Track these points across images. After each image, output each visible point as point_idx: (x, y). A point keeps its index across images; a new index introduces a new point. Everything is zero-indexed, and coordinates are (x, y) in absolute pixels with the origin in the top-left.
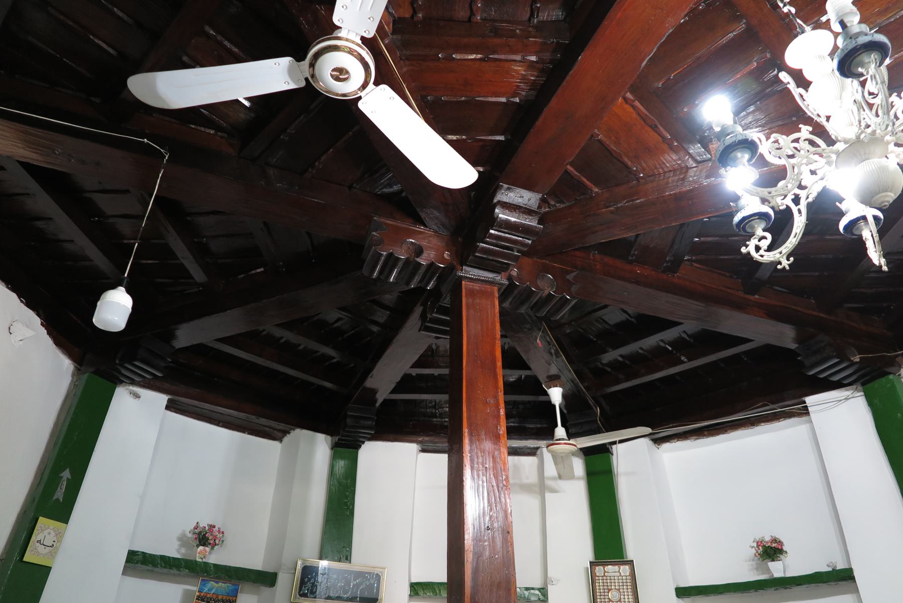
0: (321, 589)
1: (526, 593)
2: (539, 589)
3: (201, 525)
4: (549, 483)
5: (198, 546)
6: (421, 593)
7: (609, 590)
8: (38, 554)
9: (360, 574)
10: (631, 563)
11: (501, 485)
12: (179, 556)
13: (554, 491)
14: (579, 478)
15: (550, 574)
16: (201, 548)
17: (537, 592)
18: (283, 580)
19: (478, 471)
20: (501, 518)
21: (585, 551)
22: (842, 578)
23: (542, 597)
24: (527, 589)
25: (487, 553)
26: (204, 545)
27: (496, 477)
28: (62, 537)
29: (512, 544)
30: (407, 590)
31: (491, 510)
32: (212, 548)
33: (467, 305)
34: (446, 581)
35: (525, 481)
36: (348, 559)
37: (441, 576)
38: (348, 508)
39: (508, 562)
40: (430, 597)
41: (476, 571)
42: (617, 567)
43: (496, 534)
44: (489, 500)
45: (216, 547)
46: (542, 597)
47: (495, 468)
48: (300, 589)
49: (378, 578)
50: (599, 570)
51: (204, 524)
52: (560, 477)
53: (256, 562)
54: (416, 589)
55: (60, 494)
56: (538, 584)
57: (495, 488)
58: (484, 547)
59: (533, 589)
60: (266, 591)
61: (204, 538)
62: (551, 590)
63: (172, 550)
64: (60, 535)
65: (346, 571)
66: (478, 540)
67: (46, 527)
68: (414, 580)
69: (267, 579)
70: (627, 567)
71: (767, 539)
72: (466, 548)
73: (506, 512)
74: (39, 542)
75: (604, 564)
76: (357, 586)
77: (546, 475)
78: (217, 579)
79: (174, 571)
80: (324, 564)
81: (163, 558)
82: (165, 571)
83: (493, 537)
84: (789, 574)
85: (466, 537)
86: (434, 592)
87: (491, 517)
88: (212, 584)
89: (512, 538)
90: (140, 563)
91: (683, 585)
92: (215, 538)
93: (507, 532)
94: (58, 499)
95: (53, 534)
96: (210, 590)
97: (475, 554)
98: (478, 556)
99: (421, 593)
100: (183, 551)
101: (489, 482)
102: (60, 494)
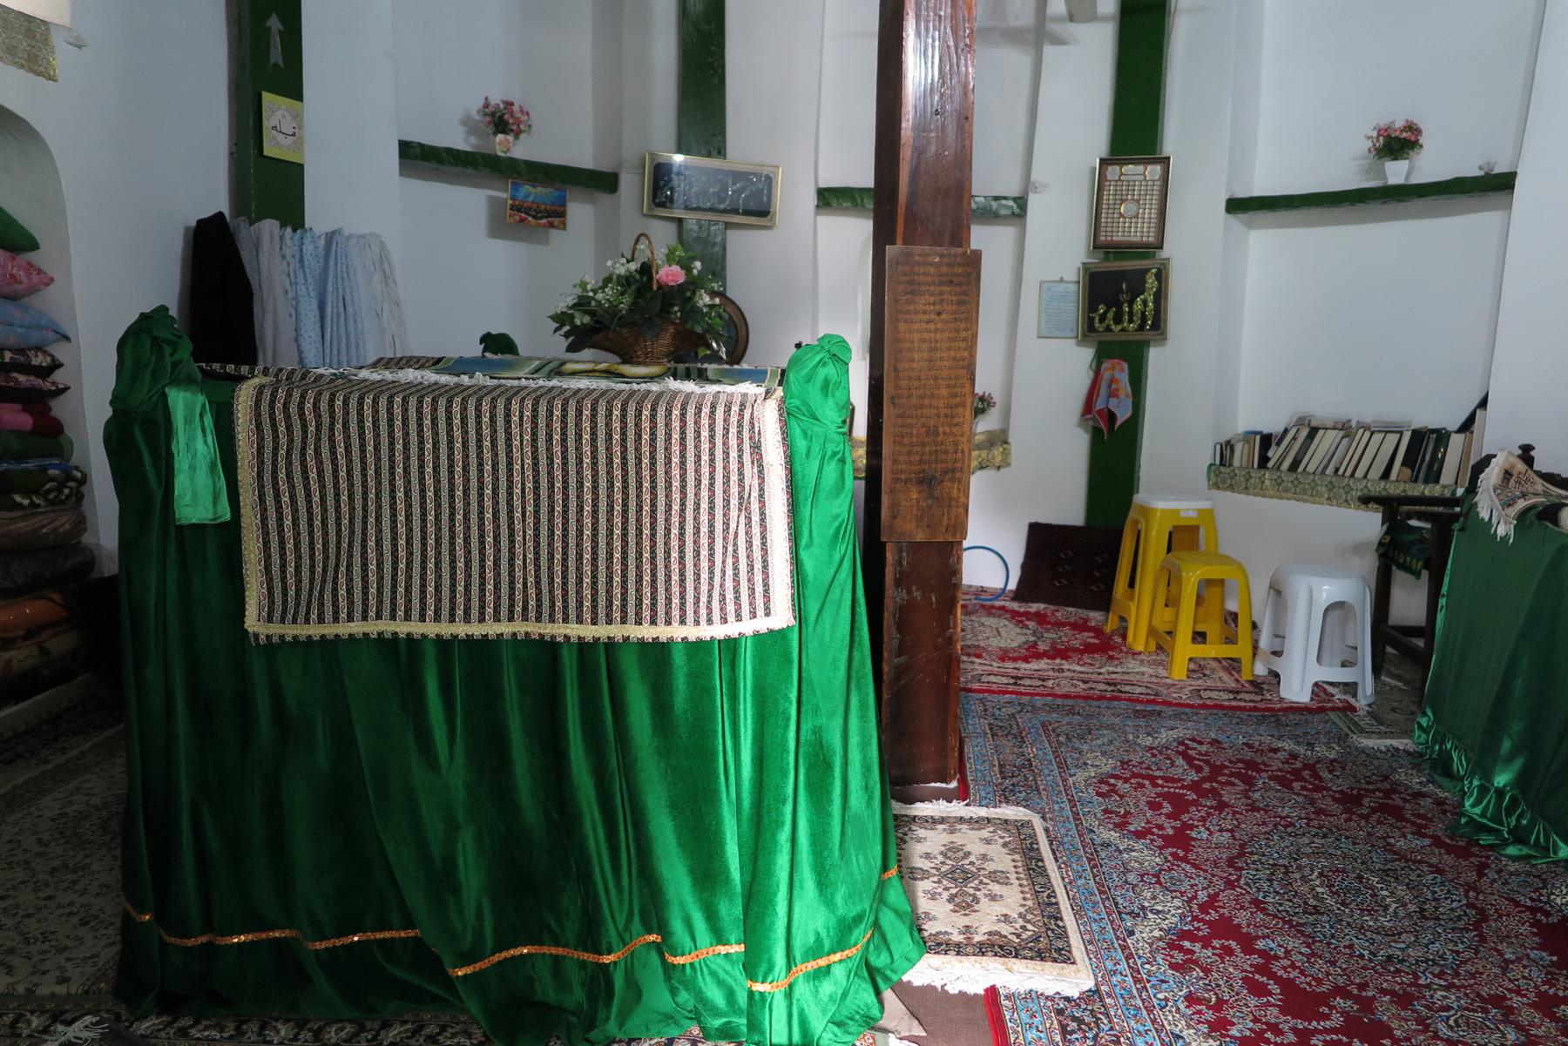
0: (679, 198)
1: (994, 204)
2: (1015, 199)
3: (493, 102)
4: (1053, 27)
5: (495, 134)
6: (834, 203)
7: (1123, 201)
8: (281, 147)
9: (738, 176)
10: (1165, 161)
11: (962, 45)
12: (468, 149)
13: (1059, 41)
14: (1105, 19)
15: (1035, 176)
16: (500, 137)
17: (1011, 203)
18: (627, 182)
19: (927, 22)
20: (957, 99)
21: (1097, 140)
22: (1497, 185)
23: (1017, 210)
24: (996, 198)
25: (933, 149)
26: (504, 132)
27: (955, 32)
28: (301, 121)
29: (971, 136)
30: (812, 199)
31: (943, 85)
32: (517, 136)
33: (836, 668)
34: (870, 184)
35: (1013, 23)
36: (721, 152)
37: (864, 177)
38: (716, 72)
39: (963, 162)
40: (847, 209)
41: (915, 174)
42: (1141, 168)
43: (948, 121)
44: (940, 69)
45: (522, 136)
46: (1017, 210)
47: (954, 17)
48: (655, 196)
49: (769, 181)
50: (1113, 172)
51: (496, 99)
52: (1071, 18)
53: (583, 157)
54: (829, 198)
55: (276, 55)
56: (1014, 191)
57: (953, 50)
58: (929, 140)
59: (1005, 198)
60: (605, 199)
61: (501, 120)
62: (1034, 202)
63: (457, 139)
64: (298, 117)
65: (718, 171)
66: (920, 128)
67: (275, 107)
68: (823, 185)
69: (603, 182)
70: (1158, 168)
71: (1399, 124)
72: (903, 140)
73: (966, 86)
74: (274, 128)
75: (1122, 163)
76: (737, 192)
77: (1049, 12)
78: (534, 181)
79: (470, 171)
80: (678, 158)
81: (449, 151)
82: (458, 169)
83: (943, 125)
84: (1415, 180)
85: (904, 125)
86: (853, 199)
87: (942, 95)
88: (526, 189)
89: (971, 126)
90: (419, 158)
91: (1242, 193)
92: (518, 122)
93: (964, 118)
94: (276, 64)
95: (289, 117)
96: (527, 195)
97: (915, 149)
98: (919, 152)
99: (834, 203)
100: (473, 140)
101: (943, 40)
102: (276, 55)
